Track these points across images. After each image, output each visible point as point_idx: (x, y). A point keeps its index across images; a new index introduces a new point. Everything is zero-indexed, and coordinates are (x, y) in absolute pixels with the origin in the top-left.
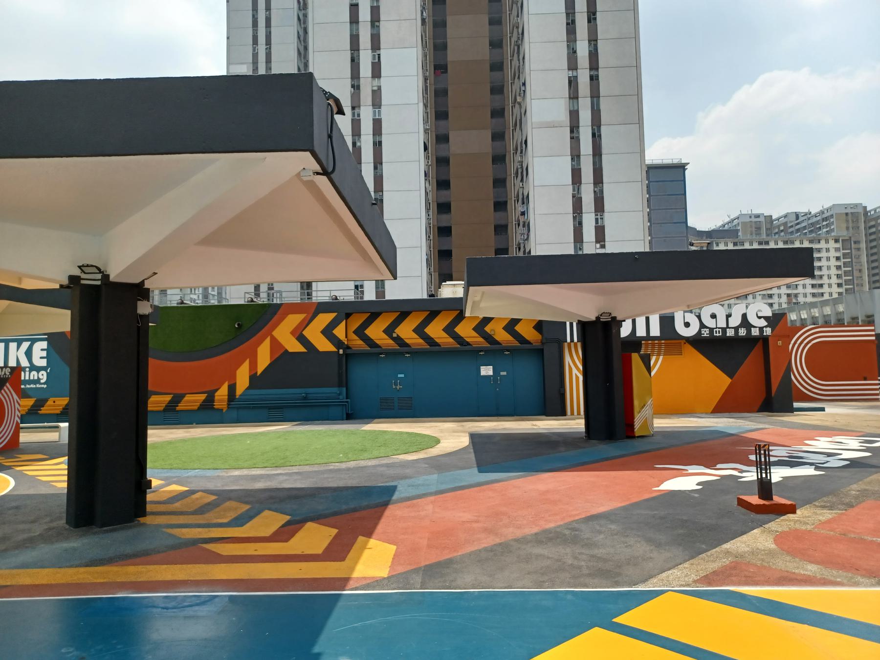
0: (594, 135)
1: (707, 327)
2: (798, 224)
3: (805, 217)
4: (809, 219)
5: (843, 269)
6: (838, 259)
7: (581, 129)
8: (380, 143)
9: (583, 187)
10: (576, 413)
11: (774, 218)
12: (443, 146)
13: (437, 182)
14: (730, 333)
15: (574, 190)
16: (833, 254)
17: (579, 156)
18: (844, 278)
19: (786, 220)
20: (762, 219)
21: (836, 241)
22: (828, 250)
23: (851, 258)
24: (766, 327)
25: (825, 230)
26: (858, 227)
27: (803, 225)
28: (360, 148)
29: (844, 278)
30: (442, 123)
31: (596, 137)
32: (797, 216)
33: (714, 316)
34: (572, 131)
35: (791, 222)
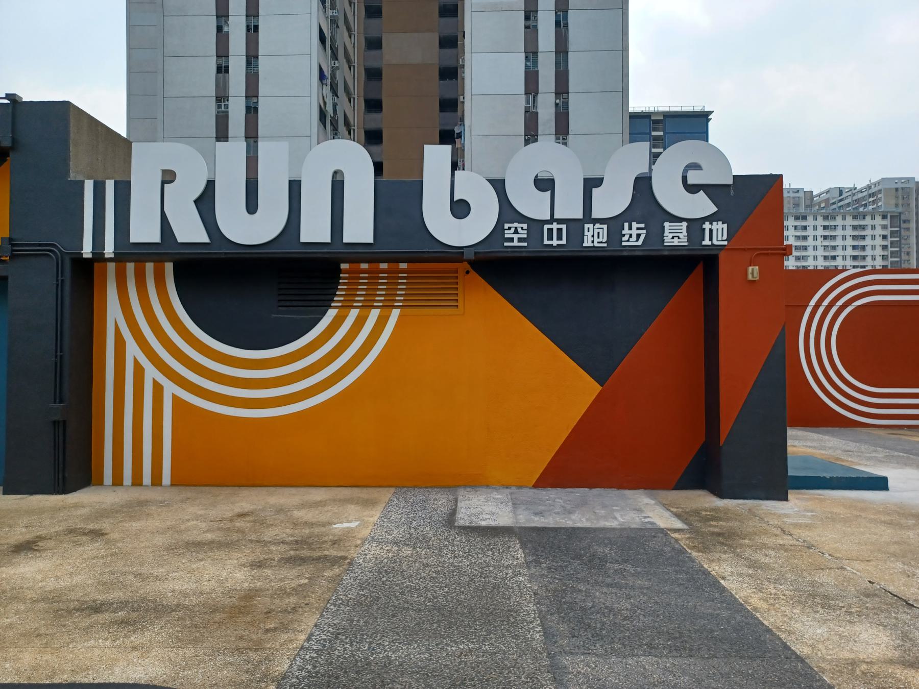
0: (558, 24)
1: (523, 218)
2: (841, 200)
3: (850, 193)
4: (854, 195)
5: (890, 249)
6: (884, 237)
7: (540, 13)
8: (256, 28)
9: (540, 97)
10: (147, 479)
11: (814, 194)
12: (374, 53)
13: (366, 101)
14: (595, 237)
15: (528, 102)
16: (879, 232)
17: (535, 53)
18: (890, 259)
19: (828, 196)
20: (801, 194)
21: (884, 217)
22: (873, 227)
23: (900, 237)
24: (711, 218)
25: (871, 207)
26: (909, 205)
27: (847, 201)
28: (227, 34)
29: (890, 259)
30: (374, 22)
31: (561, 25)
32: (841, 192)
33: (545, 184)
34: (527, 18)
35: (833, 198)
